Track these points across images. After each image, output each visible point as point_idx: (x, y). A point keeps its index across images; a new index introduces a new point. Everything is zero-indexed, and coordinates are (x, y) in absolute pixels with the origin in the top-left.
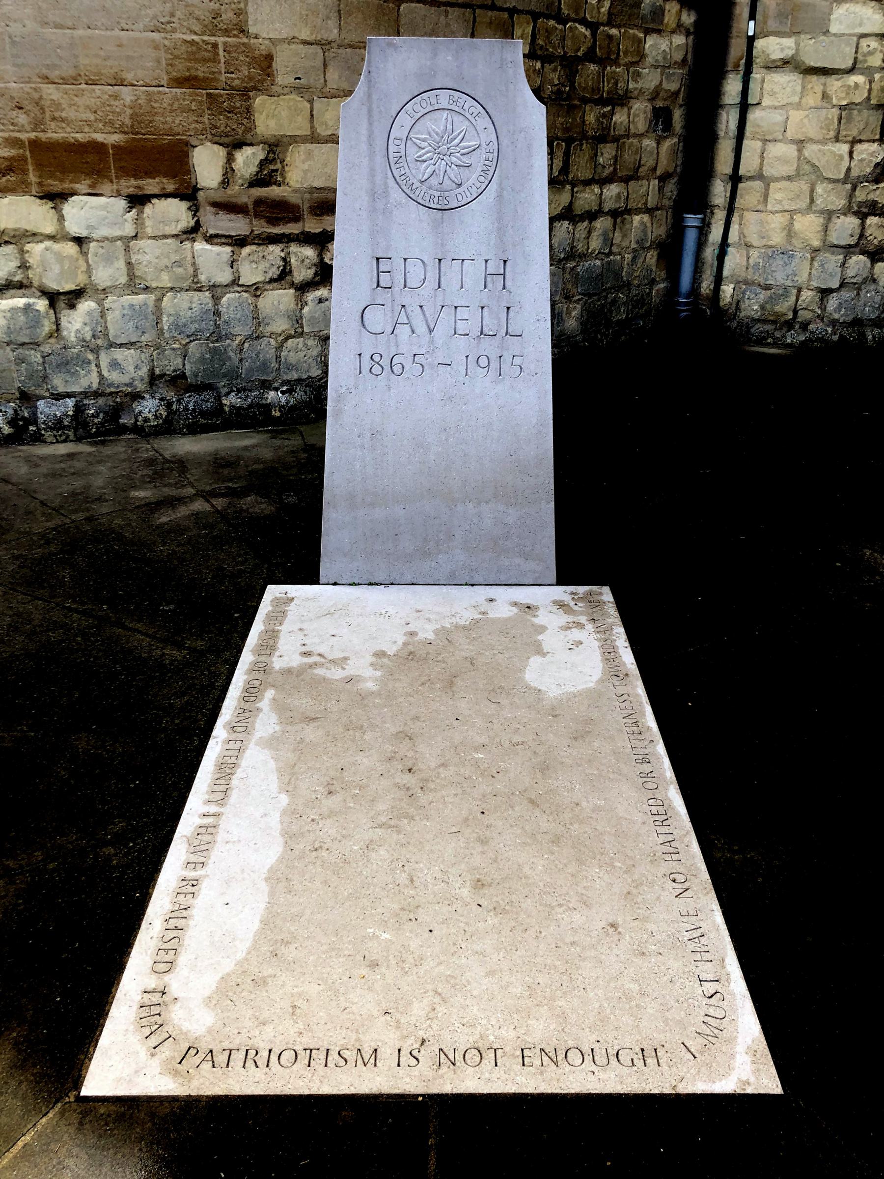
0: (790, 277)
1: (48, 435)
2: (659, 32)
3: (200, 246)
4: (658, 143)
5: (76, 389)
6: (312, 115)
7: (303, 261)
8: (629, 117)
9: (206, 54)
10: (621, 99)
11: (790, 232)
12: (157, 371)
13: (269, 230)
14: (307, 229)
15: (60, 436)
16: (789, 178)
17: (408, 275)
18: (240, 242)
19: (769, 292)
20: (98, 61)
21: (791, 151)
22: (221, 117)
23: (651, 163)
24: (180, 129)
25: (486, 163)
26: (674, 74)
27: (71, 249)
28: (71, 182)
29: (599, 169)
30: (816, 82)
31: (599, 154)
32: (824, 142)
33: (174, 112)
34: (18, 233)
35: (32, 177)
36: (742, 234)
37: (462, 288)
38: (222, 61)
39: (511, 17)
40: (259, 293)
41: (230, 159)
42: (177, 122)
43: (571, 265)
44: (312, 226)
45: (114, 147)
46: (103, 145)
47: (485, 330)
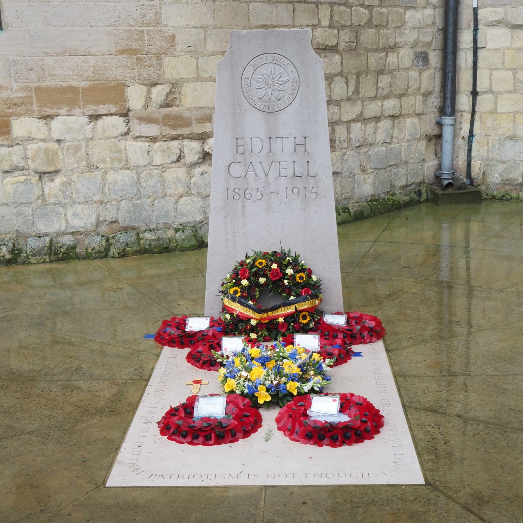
0: (517, 155)
1: (33, 260)
2: (415, 8)
4: (420, 73)
7: (192, 150)
8: (398, 59)
9: (137, 36)
10: (393, 48)
12: (101, 219)
13: (172, 133)
14: (194, 132)
15: (40, 259)
16: (509, 92)
17: (253, 146)
18: (154, 140)
19: (504, 165)
21: (509, 74)
22: (145, 70)
23: (416, 86)
25: (293, 88)
26: (427, 32)
28: (57, 109)
29: (380, 91)
31: (379, 81)
33: (118, 69)
34: (24, 139)
35: (35, 107)
37: (282, 152)
38: (146, 39)
39: (317, 6)
40: (164, 170)
41: (149, 92)
42: (119, 73)
43: (363, 150)
44: (197, 129)
45: (83, 89)
47: (296, 174)
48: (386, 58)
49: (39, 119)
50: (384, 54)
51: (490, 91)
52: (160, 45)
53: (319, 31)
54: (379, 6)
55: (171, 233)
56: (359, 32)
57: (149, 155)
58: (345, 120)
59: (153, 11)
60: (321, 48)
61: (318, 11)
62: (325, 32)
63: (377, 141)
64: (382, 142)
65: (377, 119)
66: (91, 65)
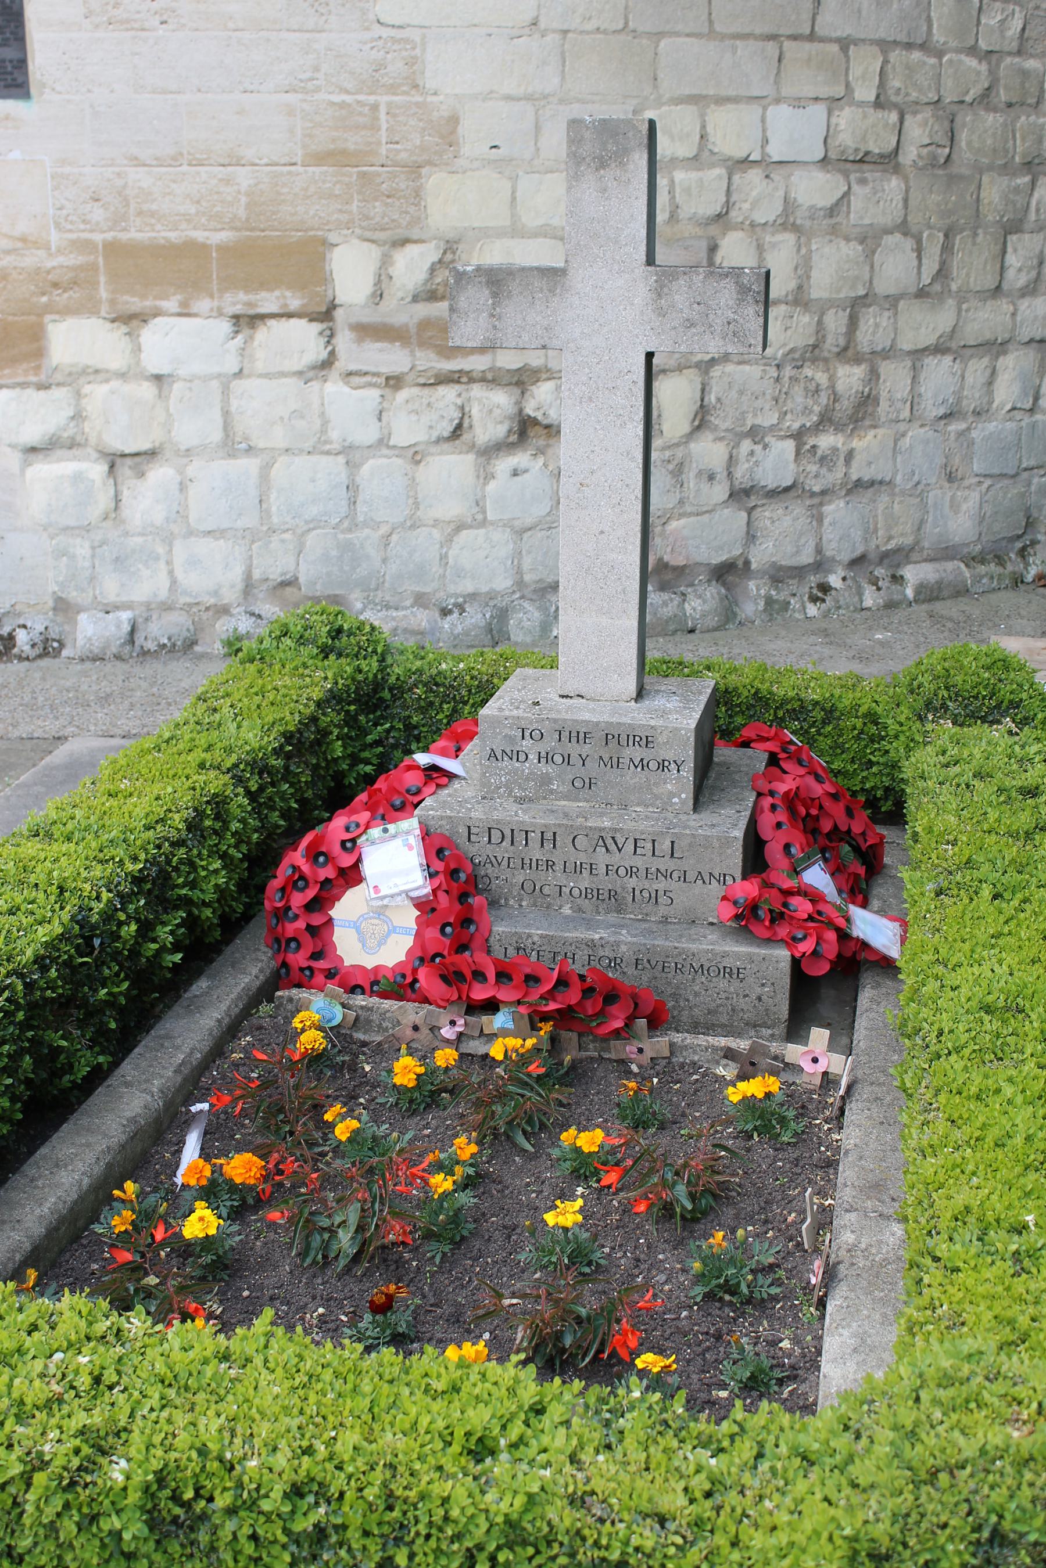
6: (514, 199)
7: (491, 411)
14: (499, 364)
18: (394, 382)
22: (377, 204)
27: (147, 390)
28: (156, 298)
31: (1009, 249)
38: (384, 126)
40: (418, 458)
41: (386, 261)
42: (312, 213)
45: (222, 248)
48: (1032, 190)
49: (113, 321)
50: (1027, 179)
52: (418, 143)
53: (844, 117)
54: (1019, 53)
55: (422, 618)
56: (958, 120)
57: (380, 420)
58: (906, 347)
59: (404, 53)
60: (851, 158)
61: (848, 61)
62: (865, 117)
63: (995, 405)
64: (1008, 407)
65: (995, 347)
66: (243, 190)
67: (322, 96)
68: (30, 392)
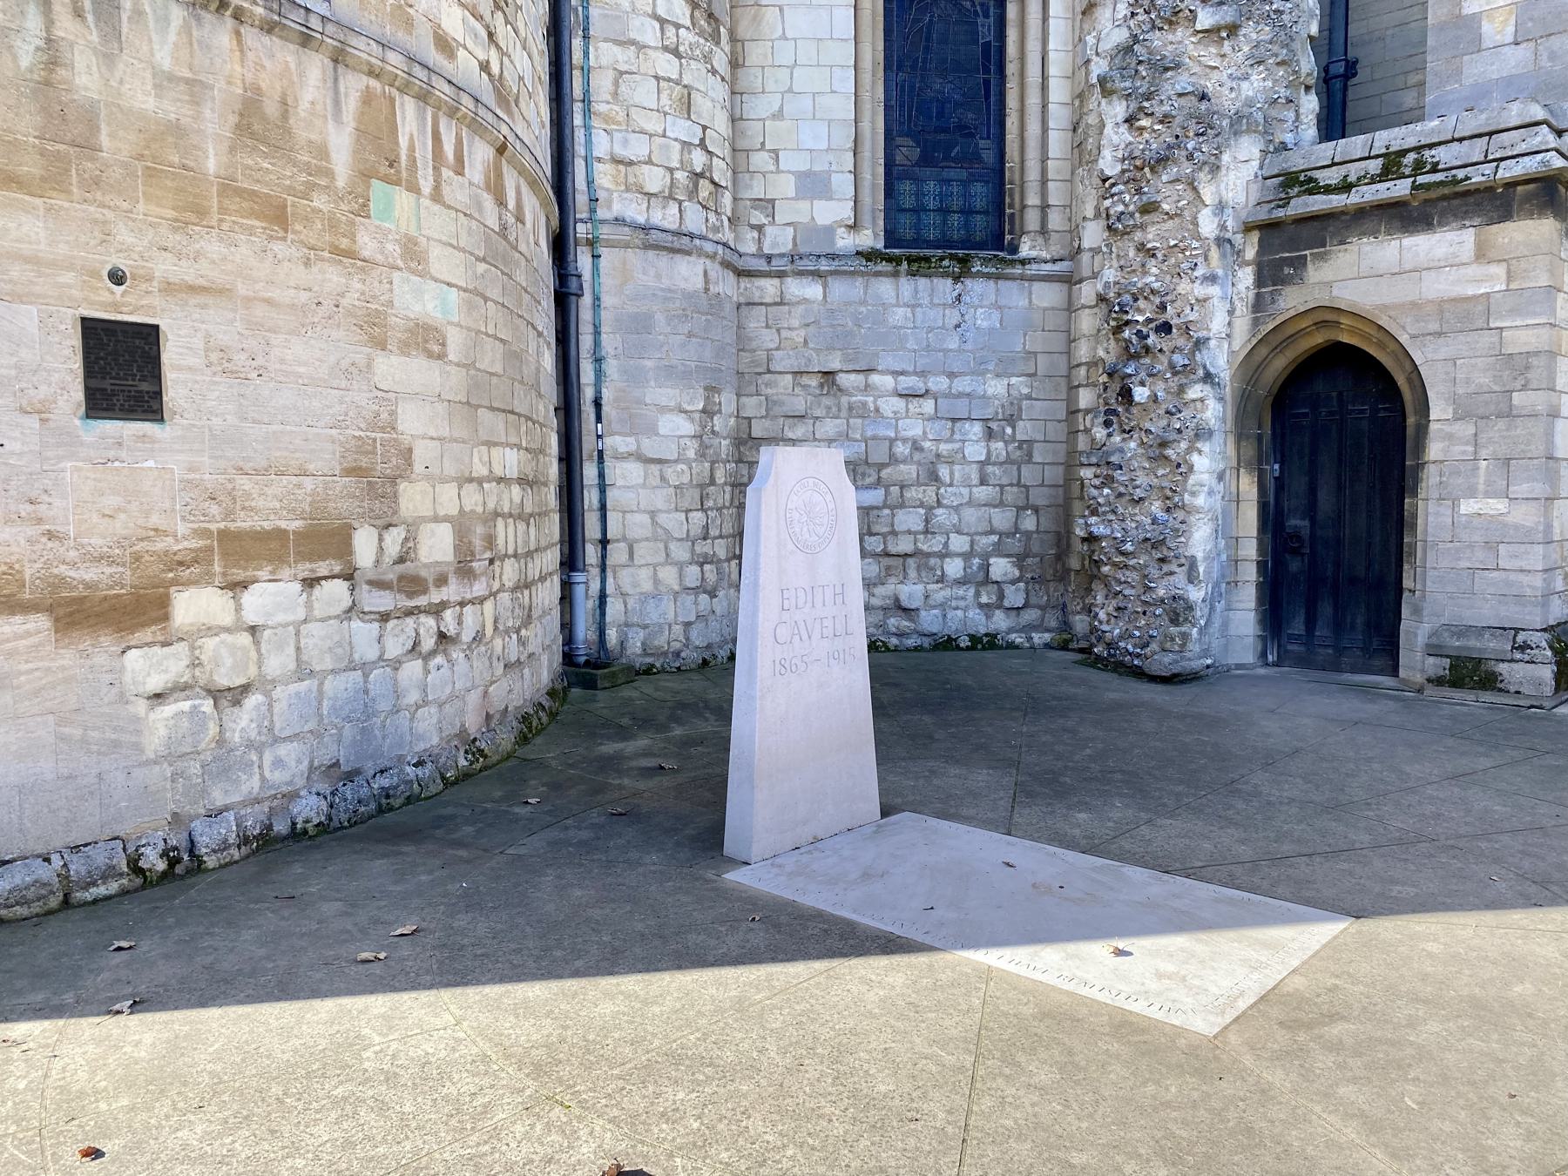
3: (356, 624)
5: (236, 798)
11: (656, 581)
12: (316, 763)
16: (647, 539)
18: (384, 617)
20: (286, 454)
24: (346, 514)
27: (245, 639)
30: (655, 468)
32: (668, 512)
33: (343, 498)
35: (217, 568)
36: (618, 587)
41: (381, 539)
46: (285, 531)
51: (624, 539)
67: (349, 431)
68: (157, 649)
